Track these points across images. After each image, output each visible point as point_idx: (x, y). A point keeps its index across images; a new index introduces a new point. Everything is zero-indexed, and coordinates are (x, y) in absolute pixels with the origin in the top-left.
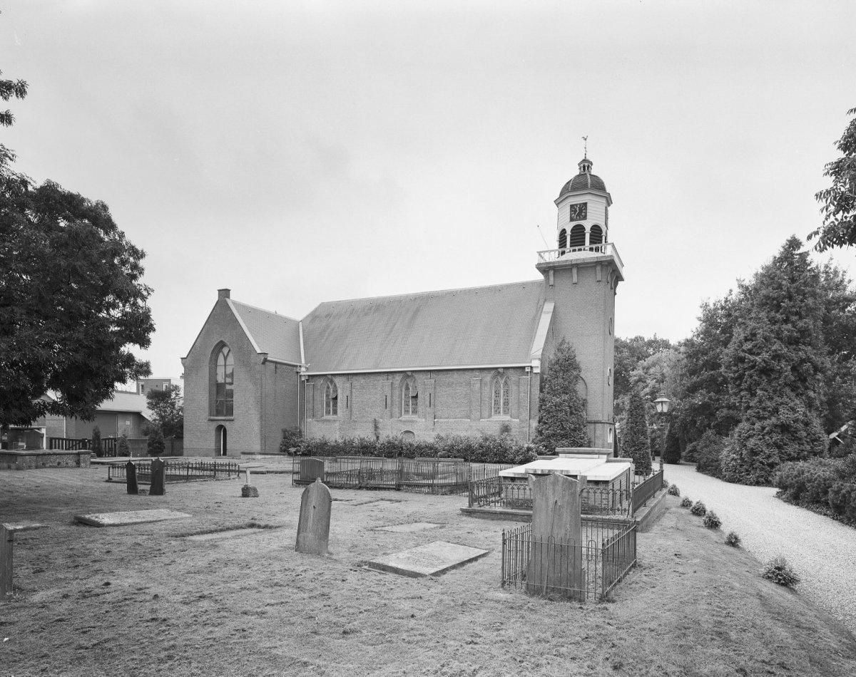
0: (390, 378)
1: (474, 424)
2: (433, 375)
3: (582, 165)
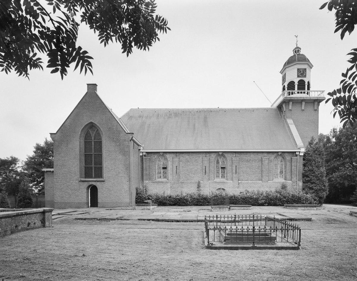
0: (207, 155)
1: (265, 184)
2: (237, 155)
3: (295, 51)
